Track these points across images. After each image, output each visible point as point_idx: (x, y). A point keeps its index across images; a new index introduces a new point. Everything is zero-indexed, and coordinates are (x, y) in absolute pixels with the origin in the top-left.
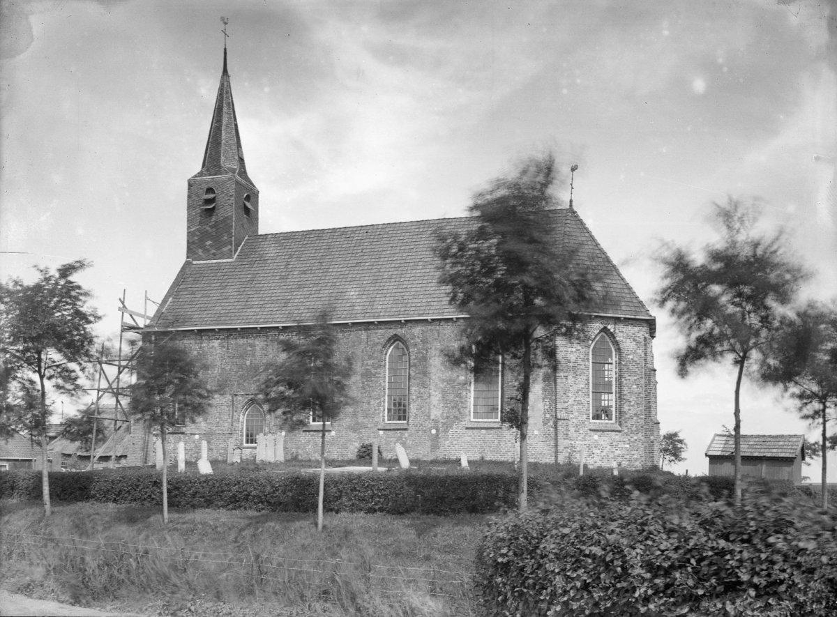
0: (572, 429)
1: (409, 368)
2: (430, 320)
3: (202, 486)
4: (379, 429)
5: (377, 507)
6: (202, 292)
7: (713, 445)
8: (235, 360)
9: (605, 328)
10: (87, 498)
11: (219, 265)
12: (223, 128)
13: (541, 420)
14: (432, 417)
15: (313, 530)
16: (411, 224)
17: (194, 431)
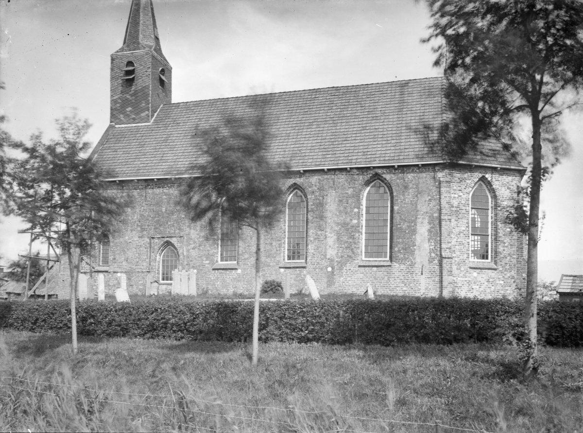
0: (454, 267)
1: (307, 212)
2: (326, 170)
3: (118, 315)
4: (280, 268)
5: (310, 336)
6: (124, 150)
7: (562, 284)
8: (152, 208)
9: (483, 177)
10: (5, 327)
11: (138, 128)
12: (141, 10)
13: (427, 259)
14: (328, 257)
15: (247, 364)
16: (304, 92)
17: (116, 270)
